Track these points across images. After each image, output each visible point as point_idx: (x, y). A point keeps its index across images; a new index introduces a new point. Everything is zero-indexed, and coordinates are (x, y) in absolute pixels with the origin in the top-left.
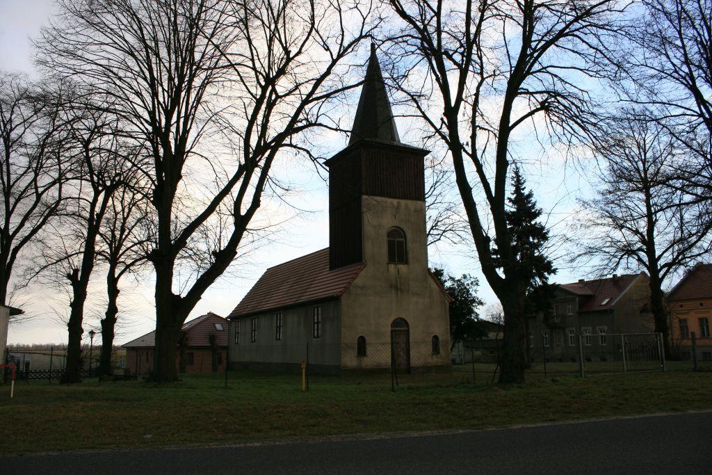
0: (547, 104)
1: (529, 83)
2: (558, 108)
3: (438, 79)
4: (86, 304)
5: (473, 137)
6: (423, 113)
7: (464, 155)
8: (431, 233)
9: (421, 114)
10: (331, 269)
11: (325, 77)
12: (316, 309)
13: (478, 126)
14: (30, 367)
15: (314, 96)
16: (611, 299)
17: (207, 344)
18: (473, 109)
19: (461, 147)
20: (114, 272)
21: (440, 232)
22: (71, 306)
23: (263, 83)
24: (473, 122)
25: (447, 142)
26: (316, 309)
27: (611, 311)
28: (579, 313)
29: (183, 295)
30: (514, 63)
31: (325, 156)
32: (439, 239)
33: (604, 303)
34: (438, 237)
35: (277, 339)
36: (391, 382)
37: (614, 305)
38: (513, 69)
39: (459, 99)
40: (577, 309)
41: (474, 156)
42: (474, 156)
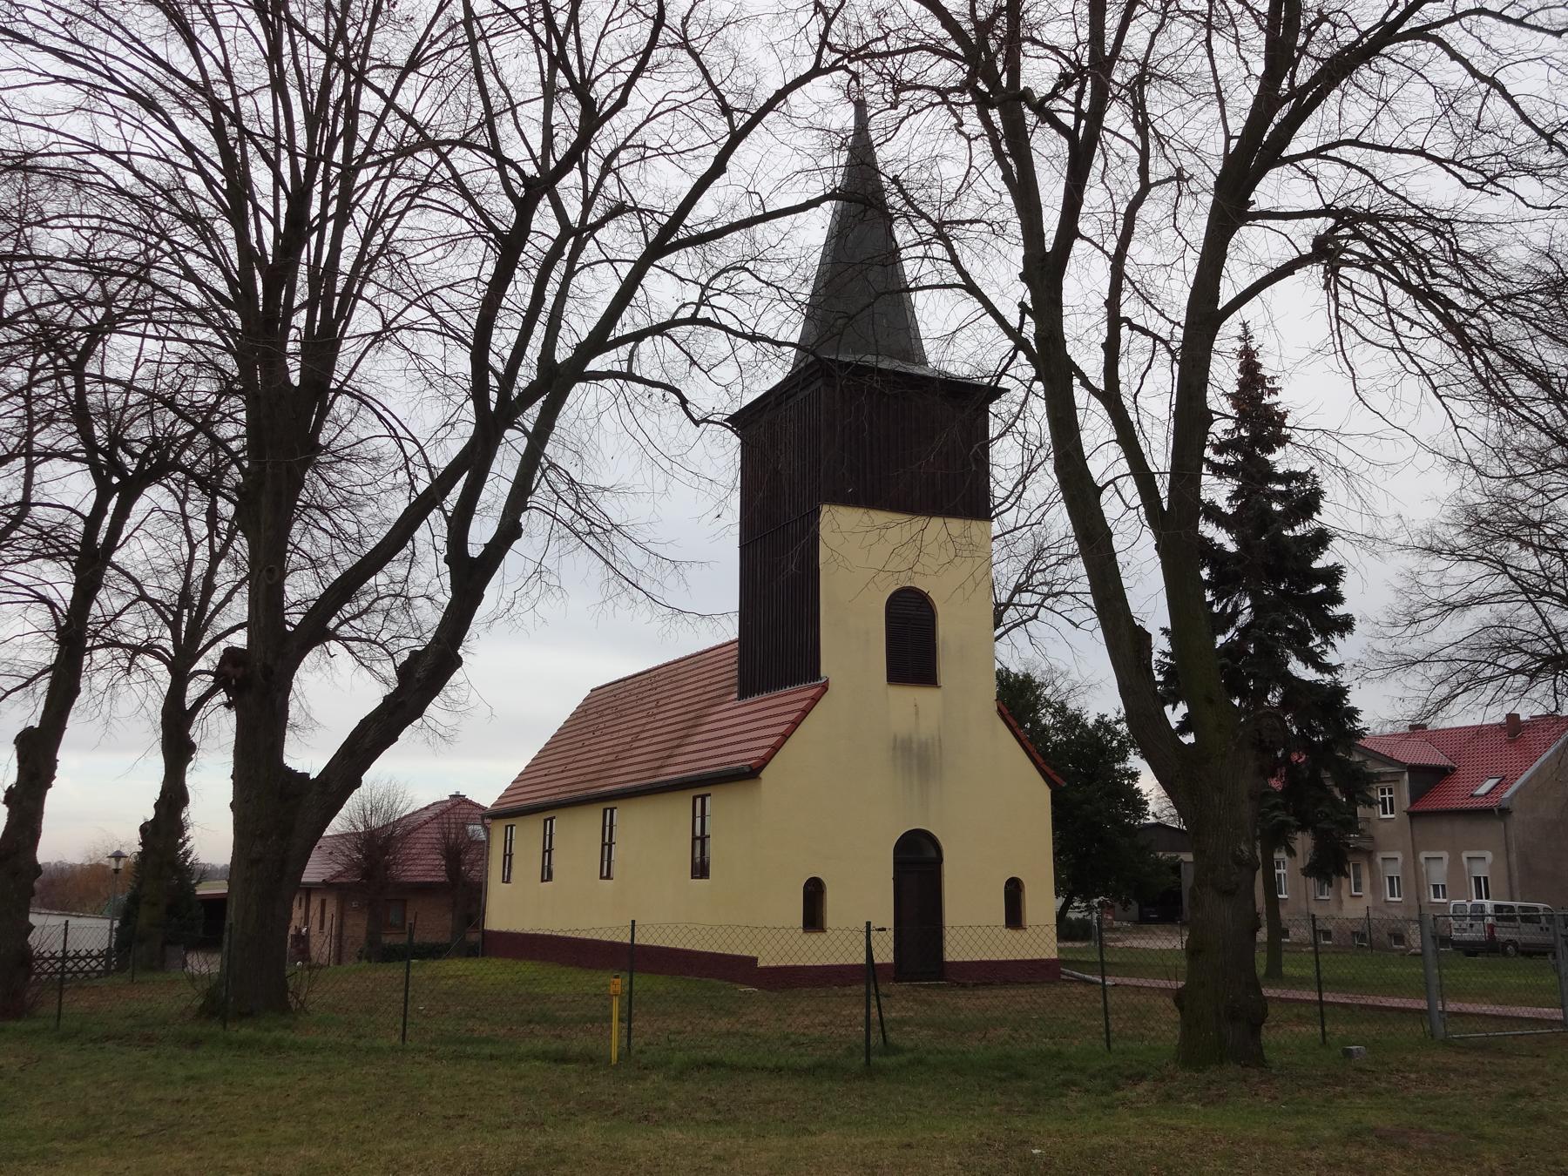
0: (1330, 246)
1: (1272, 190)
2: (1397, 254)
3: (1007, 178)
4: (52, 798)
5: (1112, 349)
6: (964, 274)
7: (1080, 395)
8: (1016, 599)
9: (959, 279)
10: (742, 696)
11: (711, 181)
12: (699, 801)
13: (1128, 320)
14: (189, 860)
15: (682, 234)
16: (1503, 781)
17: (440, 876)
18: (1112, 268)
19: (1071, 368)
20: (184, 690)
21: (1036, 599)
22: (7, 801)
23: (521, 192)
24: (1113, 303)
25: (446, 518)
26: (699, 801)
27: (1504, 812)
28: (1413, 815)
29: (313, 776)
30: (1237, 125)
31: (1269, 263)
32: (1035, 617)
33: (1483, 790)
34: (1031, 612)
35: (601, 878)
36: (860, 1011)
37: (1511, 798)
38: (1234, 143)
39: (1069, 230)
40: (1406, 804)
41: (1110, 397)
42: (1110, 397)
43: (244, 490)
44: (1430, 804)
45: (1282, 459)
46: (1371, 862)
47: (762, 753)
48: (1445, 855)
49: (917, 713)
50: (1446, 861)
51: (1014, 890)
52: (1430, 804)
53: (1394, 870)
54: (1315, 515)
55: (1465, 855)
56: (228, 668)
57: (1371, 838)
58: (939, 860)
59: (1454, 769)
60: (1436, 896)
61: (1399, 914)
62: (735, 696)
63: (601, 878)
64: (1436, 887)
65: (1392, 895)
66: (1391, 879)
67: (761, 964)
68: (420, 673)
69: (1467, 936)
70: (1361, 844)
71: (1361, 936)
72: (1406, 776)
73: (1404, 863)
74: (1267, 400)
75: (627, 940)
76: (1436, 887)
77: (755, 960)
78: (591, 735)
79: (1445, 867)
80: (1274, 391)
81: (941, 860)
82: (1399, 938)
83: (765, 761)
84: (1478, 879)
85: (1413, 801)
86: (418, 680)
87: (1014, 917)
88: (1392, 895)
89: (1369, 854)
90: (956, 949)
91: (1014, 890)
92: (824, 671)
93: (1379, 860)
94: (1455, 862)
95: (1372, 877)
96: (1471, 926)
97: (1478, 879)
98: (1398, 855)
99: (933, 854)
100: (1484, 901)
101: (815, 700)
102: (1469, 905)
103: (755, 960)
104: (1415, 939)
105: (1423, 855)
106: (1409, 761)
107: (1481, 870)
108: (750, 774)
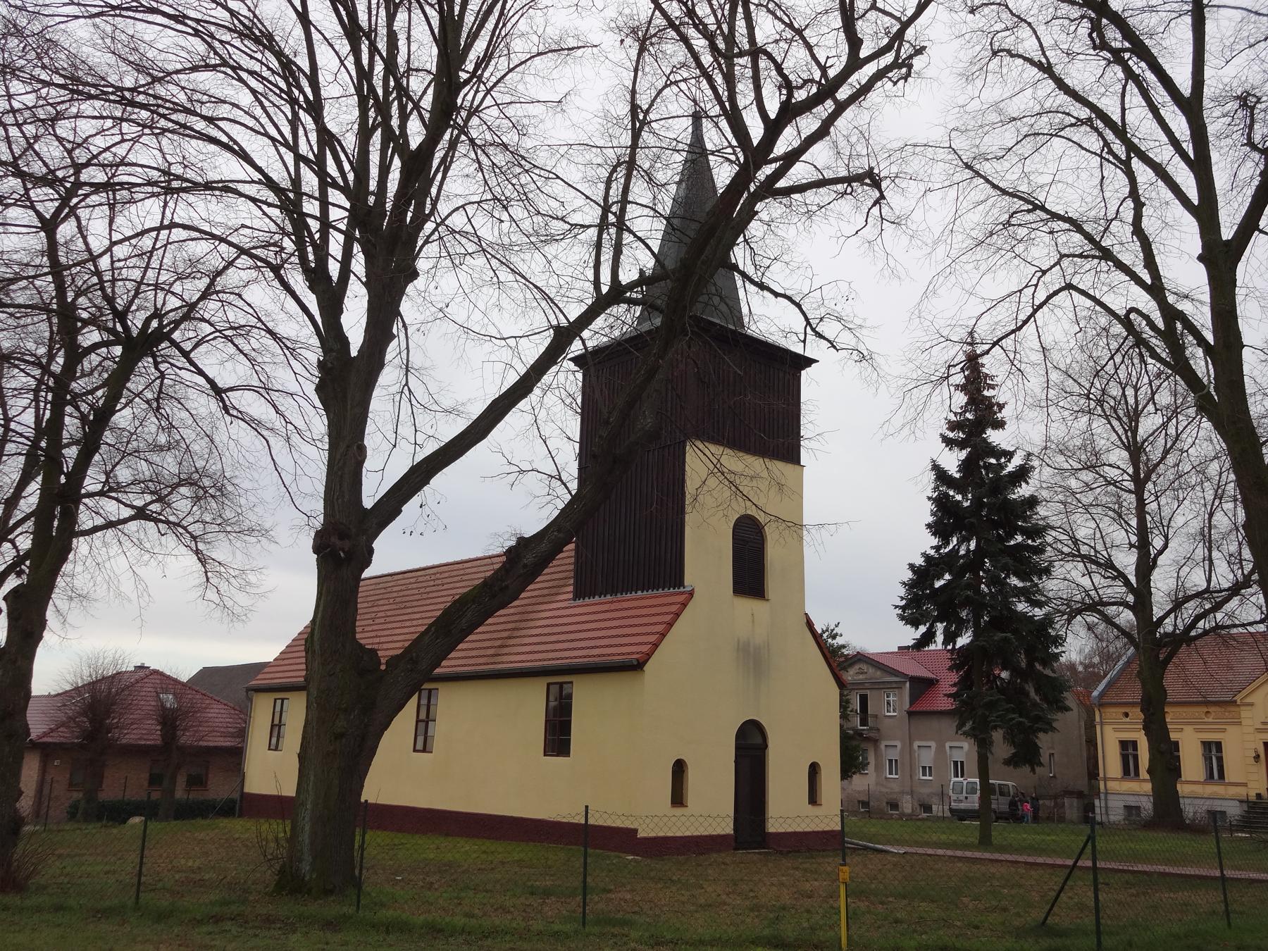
28: (911, 714)
35: (415, 750)
40: (907, 706)
43: (329, 365)
44: (923, 706)
45: (994, 437)
46: (877, 748)
47: (645, 648)
48: (933, 744)
49: (753, 622)
50: (933, 749)
51: (814, 769)
52: (923, 706)
53: (894, 754)
54: (1023, 484)
55: (948, 745)
56: (334, 540)
57: (878, 730)
58: (764, 746)
59: (937, 681)
60: (924, 774)
61: (896, 788)
62: (571, 596)
63: (415, 750)
64: (924, 768)
65: (891, 773)
66: (891, 761)
67: (641, 834)
68: (529, 559)
69: (963, 806)
70: (871, 735)
71: (865, 804)
72: (908, 684)
73: (902, 749)
74: (986, 393)
75: (583, 822)
76: (924, 768)
77: (635, 831)
78: (370, 622)
79: (933, 753)
80: (992, 387)
81: (766, 746)
82: (894, 806)
83: (649, 656)
84: (956, 763)
85: (911, 704)
86: (525, 566)
87: (813, 799)
88: (891, 773)
89: (875, 742)
90: (773, 826)
91: (814, 769)
92: (688, 580)
93: (882, 747)
94: (940, 749)
95: (876, 760)
96: (966, 798)
97: (956, 763)
98: (898, 744)
99: (759, 740)
100: (960, 779)
101: (684, 605)
102: (965, 782)
103: (635, 831)
104: (907, 806)
105: (916, 744)
106: (911, 674)
107: (959, 756)
108: (636, 666)
